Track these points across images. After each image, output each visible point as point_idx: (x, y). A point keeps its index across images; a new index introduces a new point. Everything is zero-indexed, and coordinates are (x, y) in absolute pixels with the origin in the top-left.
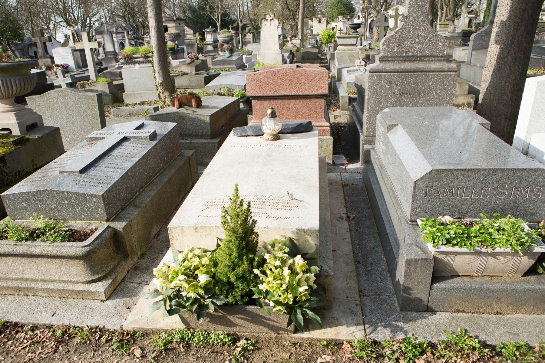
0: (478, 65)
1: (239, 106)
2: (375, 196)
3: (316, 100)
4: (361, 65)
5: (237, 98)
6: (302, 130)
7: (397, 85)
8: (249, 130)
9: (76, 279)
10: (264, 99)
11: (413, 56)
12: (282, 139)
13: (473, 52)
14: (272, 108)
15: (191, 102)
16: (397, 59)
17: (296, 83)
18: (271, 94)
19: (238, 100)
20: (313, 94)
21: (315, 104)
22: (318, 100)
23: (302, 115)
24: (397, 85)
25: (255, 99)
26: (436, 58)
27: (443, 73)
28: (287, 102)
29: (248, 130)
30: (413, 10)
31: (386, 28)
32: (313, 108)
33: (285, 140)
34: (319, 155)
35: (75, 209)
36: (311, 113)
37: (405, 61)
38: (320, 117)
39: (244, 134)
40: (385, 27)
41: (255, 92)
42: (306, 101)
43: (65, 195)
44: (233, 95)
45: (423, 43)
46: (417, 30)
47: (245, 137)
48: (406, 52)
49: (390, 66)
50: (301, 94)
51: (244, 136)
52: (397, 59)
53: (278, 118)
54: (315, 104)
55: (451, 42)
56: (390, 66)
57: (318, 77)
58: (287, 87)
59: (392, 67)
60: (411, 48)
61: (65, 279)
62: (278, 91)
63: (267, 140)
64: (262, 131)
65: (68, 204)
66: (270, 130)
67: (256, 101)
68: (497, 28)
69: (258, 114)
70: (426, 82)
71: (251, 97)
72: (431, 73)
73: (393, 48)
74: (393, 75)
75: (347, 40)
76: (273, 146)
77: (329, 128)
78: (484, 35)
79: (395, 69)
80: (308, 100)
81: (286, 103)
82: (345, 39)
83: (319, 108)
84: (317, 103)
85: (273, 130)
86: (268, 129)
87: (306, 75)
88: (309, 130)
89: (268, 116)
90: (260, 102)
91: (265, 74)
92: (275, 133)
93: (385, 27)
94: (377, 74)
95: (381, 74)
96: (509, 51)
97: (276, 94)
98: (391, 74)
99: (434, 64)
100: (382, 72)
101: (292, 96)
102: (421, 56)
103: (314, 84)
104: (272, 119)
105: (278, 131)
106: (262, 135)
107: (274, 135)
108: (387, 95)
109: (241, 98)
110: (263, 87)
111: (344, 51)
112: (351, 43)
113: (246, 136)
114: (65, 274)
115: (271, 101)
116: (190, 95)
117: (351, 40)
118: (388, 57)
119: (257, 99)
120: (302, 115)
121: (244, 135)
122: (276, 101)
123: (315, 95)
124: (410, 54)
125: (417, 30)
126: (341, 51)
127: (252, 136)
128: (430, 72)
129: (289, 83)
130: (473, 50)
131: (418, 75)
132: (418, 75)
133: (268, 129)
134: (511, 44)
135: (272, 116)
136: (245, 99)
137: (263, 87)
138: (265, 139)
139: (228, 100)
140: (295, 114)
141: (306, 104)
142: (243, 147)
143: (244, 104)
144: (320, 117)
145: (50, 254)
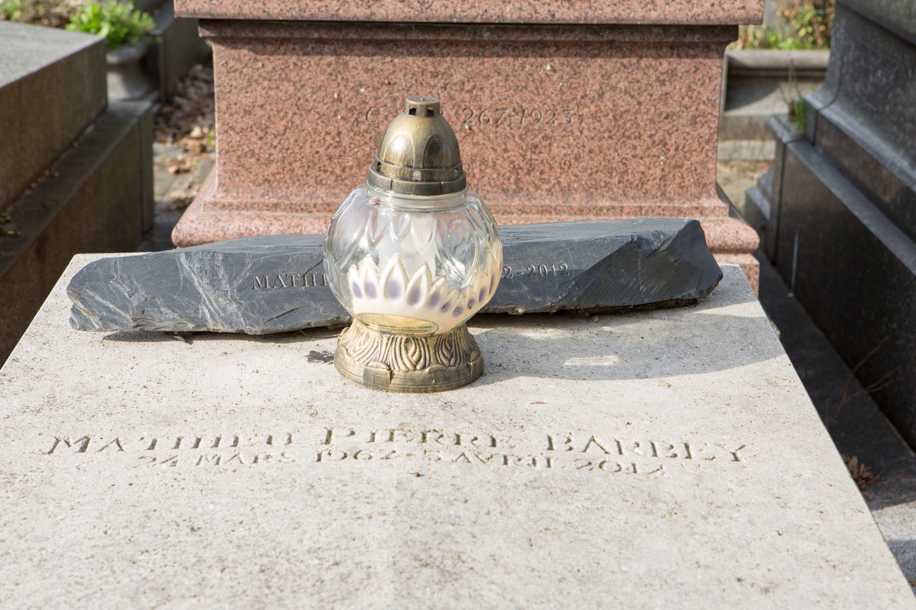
1: (102, 89)
3: (665, 65)
5: (89, 40)
6: (646, 292)
8: (214, 282)
10: (303, 41)
12: (503, 371)
14: (431, 112)
19: (95, 52)
20: (654, 16)
21: (658, 91)
22: (683, 65)
23: (565, 167)
25: (231, 42)
29: (200, 284)
32: (642, 120)
33: (524, 382)
36: (627, 152)
38: (689, 180)
39: (168, 320)
44: (63, 22)
47: (179, 345)
51: (169, 335)
53: (472, 200)
54: (658, 91)
63: (372, 381)
64: (328, 297)
66: (414, 297)
67: (245, 52)
69: (257, 146)
71: (206, 22)
76: (446, 453)
77: (750, 260)
81: (458, 77)
83: (686, 117)
84: (678, 88)
85: (433, 300)
86: (392, 291)
88: (692, 293)
89: (391, 173)
90: (270, 63)
92: (446, 323)
99: (301, 32)
101: (501, 27)
104: (428, 202)
105: (477, 308)
106: (336, 327)
107: (445, 342)
109: (112, 42)
113: (189, 337)
115: (353, 61)
119: (248, 42)
120: (565, 167)
121: (168, 326)
122: (384, 64)
123: (666, 28)
127: (240, 335)
133: (392, 291)
135: (428, 176)
136: (133, 52)
138: (356, 368)
139: (33, 45)
140: (513, 155)
141: (594, 86)
142: (164, 449)
143: (128, 82)
144: (689, 180)
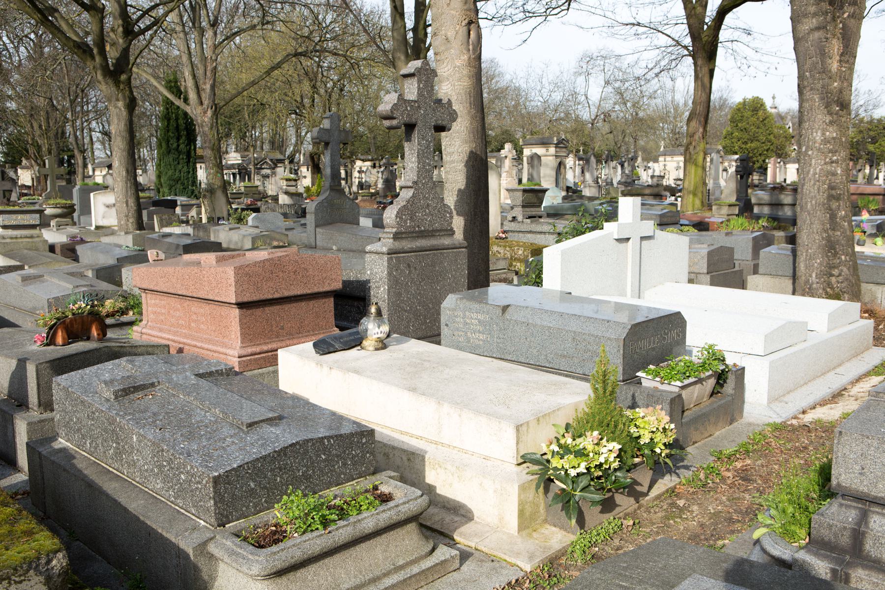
0: (334, 248)
2: (153, 529)
4: (159, 258)
7: (415, 268)
9: (415, 555)
11: (424, 231)
13: (318, 230)
15: (89, 330)
16: (410, 235)
17: (303, 276)
18: (270, 297)
24: (415, 268)
26: (445, 233)
27: (455, 250)
28: (287, 307)
30: (422, 175)
31: (7, 194)
34: (706, 284)
35: (333, 466)
37: (418, 237)
40: (4, 191)
41: (248, 295)
42: (312, 303)
43: (324, 444)
45: (432, 215)
46: (427, 199)
48: (418, 227)
49: (407, 244)
50: (309, 292)
52: (410, 235)
55: (164, 217)
56: (407, 244)
57: (329, 266)
58: (291, 283)
59: (409, 246)
60: (423, 220)
61: (401, 562)
62: (279, 290)
65: (325, 460)
67: (245, 310)
68: (455, 196)
70: (441, 262)
72: (445, 251)
73: (405, 222)
74: (411, 256)
75: (20, 216)
78: (326, 204)
79: (412, 248)
80: (314, 302)
82: (14, 216)
87: (314, 262)
91: (261, 265)
93: (4, 191)
94: (395, 255)
95: (399, 255)
96: (475, 223)
97: (277, 296)
98: (409, 254)
100: (400, 253)
102: (432, 231)
103: (324, 275)
108: (407, 283)
110: (259, 285)
111: (14, 240)
112: (28, 223)
114: (398, 556)
115: (266, 308)
116: (90, 316)
117: (28, 216)
118: (402, 233)
124: (423, 228)
125: (427, 199)
126: (8, 241)
128: (444, 249)
129: (294, 276)
130: (316, 226)
131: (434, 255)
132: (434, 255)
134: (475, 215)
137: (259, 285)
145: (388, 523)
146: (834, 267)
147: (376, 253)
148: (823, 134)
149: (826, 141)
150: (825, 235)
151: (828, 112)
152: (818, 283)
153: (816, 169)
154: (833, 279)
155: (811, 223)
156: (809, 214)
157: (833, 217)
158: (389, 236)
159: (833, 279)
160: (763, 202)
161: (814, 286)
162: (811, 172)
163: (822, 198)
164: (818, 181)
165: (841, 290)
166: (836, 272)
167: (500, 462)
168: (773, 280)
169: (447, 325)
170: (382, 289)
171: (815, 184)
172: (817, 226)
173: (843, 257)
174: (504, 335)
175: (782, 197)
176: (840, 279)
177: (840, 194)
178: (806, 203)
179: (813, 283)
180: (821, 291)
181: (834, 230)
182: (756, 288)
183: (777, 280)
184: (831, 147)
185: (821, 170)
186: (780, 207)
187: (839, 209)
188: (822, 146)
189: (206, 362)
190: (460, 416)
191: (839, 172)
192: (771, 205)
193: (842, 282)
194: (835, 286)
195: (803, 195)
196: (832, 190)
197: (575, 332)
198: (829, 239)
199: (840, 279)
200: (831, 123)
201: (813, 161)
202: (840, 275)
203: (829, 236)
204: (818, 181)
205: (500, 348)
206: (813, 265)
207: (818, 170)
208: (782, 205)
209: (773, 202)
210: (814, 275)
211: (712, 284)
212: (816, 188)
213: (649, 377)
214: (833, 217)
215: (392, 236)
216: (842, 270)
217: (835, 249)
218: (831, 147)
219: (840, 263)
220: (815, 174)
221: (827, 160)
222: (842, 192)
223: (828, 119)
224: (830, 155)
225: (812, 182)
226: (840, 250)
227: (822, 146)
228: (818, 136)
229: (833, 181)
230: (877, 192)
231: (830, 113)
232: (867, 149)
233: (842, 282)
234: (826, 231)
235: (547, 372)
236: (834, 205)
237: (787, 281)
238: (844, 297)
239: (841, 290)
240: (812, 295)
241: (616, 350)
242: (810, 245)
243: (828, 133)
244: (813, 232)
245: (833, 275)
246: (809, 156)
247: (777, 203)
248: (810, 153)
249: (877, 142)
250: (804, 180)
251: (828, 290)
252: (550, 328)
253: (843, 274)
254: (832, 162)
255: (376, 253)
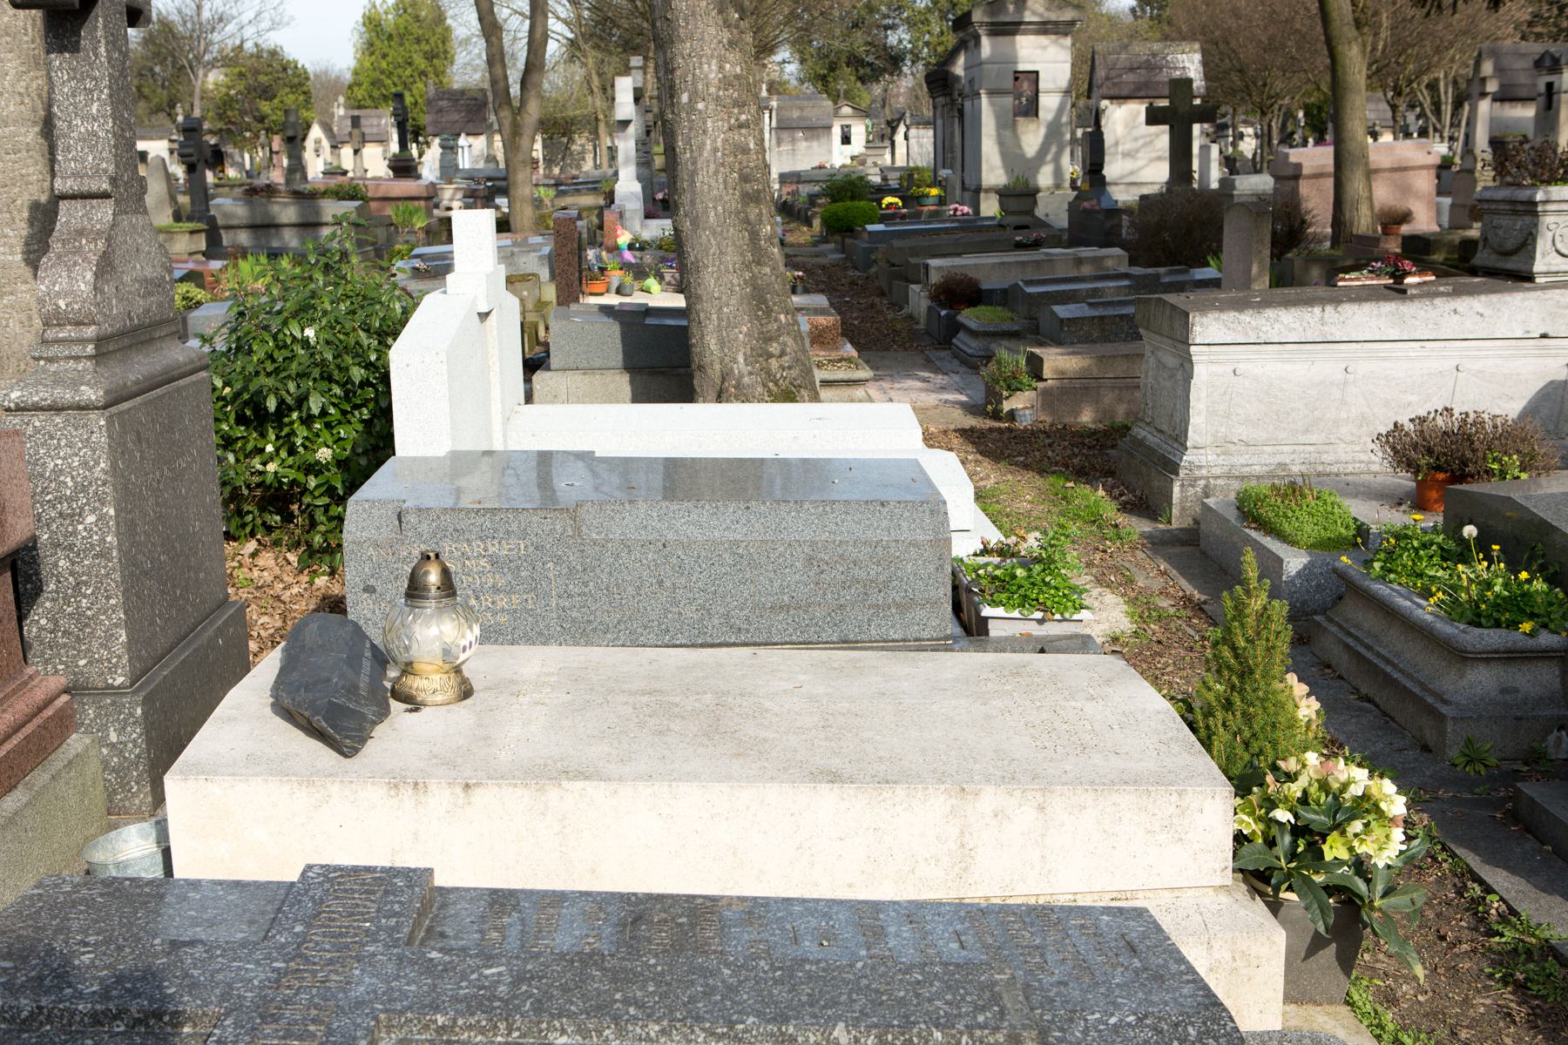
49: (141, 366)
56: (141, 366)
68: (24, 225)
146: (771, 339)
147: (50, 408)
148: (721, 68)
149: (726, 83)
150: (747, 275)
151: (724, 22)
152: (750, 373)
153: (715, 141)
154: (774, 363)
155: (721, 253)
156: (714, 233)
157: (754, 236)
158: (77, 350)
159: (774, 363)
160: (235, 222)
161: (746, 380)
162: (708, 147)
163: (732, 200)
164: (723, 165)
165: (791, 383)
166: (774, 348)
167: (1166, 894)
168: (587, 379)
169: (369, 589)
170: (91, 519)
171: (716, 172)
172: (731, 258)
173: (782, 317)
174: (586, 584)
175: (276, 209)
176: (786, 361)
177: (758, 191)
178: (706, 212)
179: (742, 376)
180: (760, 389)
181: (758, 263)
182: (554, 399)
183: (597, 379)
184: (736, 95)
185: (725, 141)
186: (273, 231)
187: (761, 220)
188: (721, 93)
189: (1512, 864)
190: (1041, 808)
191: (752, 146)
192: (253, 227)
193: (790, 368)
194: (778, 376)
195: (694, 192)
196: (746, 182)
197: (813, 544)
198: (753, 283)
199: (786, 361)
200: (732, 44)
201: (709, 124)
202: (783, 354)
203: (754, 278)
204: (723, 165)
205: (574, 620)
206: (736, 339)
207: (719, 144)
208: (278, 226)
209: (258, 222)
210: (741, 359)
211: (637, 399)
212: (721, 180)
213: (1016, 614)
214: (754, 236)
215: (90, 349)
216: (785, 344)
217: (765, 302)
218: (736, 95)
219: (779, 329)
220: (715, 150)
221: (733, 121)
222: (760, 187)
223: (726, 36)
224: (736, 111)
225: (712, 167)
226: (775, 304)
227: (721, 93)
228: (711, 71)
229: (745, 164)
230: (414, 193)
231: (727, 24)
232: (257, 109)
233: (790, 368)
234: (748, 267)
235: (883, 649)
236: (753, 212)
237: (618, 378)
238: (802, 397)
239: (791, 383)
240: (746, 399)
241: (932, 568)
242: (724, 298)
243: (728, 66)
244: (727, 271)
245: (771, 356)
246: (700, 112)
247: (266, 222)
248: (700, 106)
249: (275, 96)
250: (695, 163)
251: (771, 384)
252: (737, 543)
253: (788, 350)
254: (740, 126)
255: (50, 408)
